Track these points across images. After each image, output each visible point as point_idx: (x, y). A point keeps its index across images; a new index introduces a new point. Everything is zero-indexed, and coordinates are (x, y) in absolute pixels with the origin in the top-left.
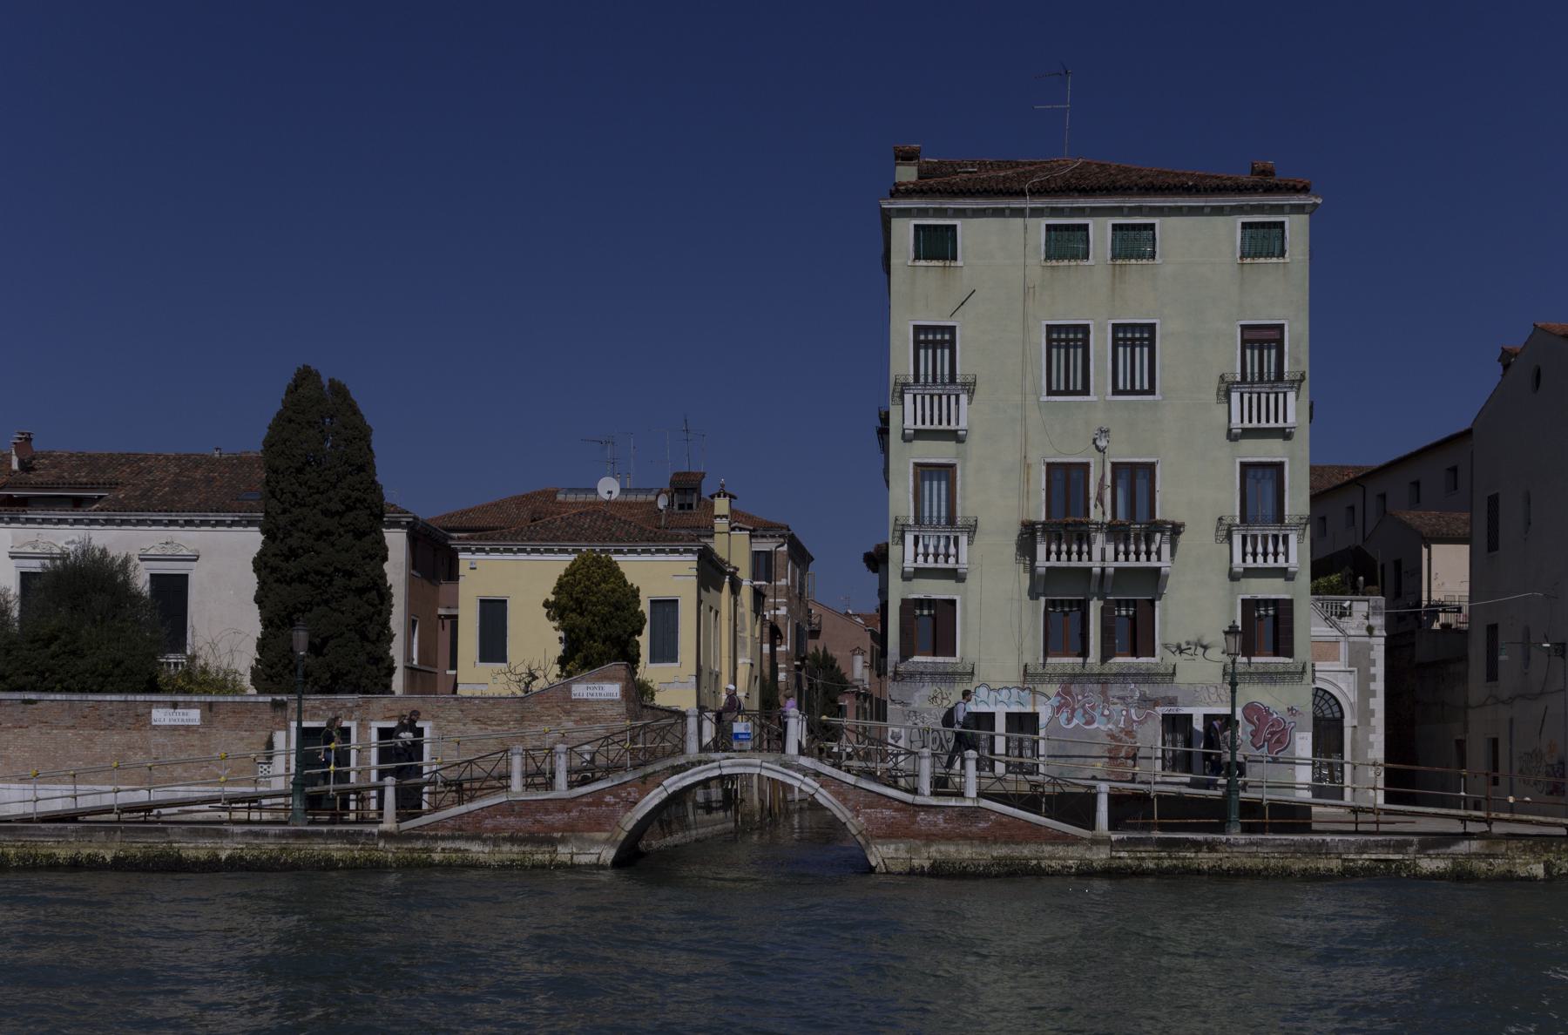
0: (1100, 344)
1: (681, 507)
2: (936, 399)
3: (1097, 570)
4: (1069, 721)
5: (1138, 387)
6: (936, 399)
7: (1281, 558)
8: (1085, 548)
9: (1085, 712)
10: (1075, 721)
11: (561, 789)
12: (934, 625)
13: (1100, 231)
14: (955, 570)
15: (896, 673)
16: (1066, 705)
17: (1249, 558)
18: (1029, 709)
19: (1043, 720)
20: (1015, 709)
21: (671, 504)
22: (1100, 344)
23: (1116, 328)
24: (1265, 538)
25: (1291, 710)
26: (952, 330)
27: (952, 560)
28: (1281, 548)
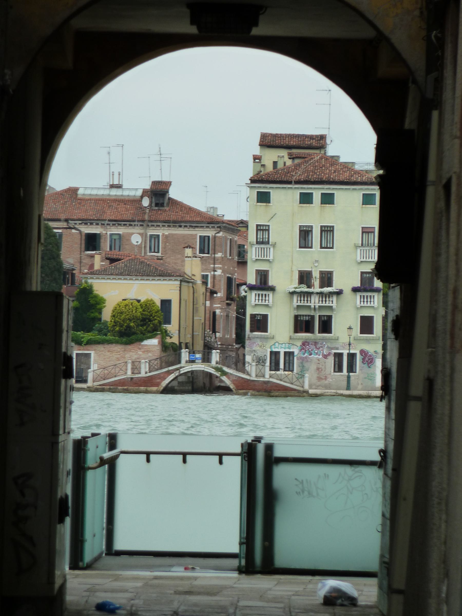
0: (316, 233)
1: (157, 205)
2: (263, 249)
3: (313, 306)
4: (304, 354)
5: (329, 246)
6: (263, 249)
7: (372, 303)
8: (309, 299)
9: (309, 352)
10: (306, 354)
11: (143, 374)
12: (260, 324)
13: (317, 197)
14: (268, 305)
15: (249, 337)
16: (303, 349)
17: (362, 303)
18: (291, 350)
19: (296, 354)
20: (287, 350)
21: (151, 203)
22: (316, 233)
23: (321, 227)
24: (262, 295)
25: (375, 352)
26: (269, 226)
27: (267, 302)
28: (372, 300)
